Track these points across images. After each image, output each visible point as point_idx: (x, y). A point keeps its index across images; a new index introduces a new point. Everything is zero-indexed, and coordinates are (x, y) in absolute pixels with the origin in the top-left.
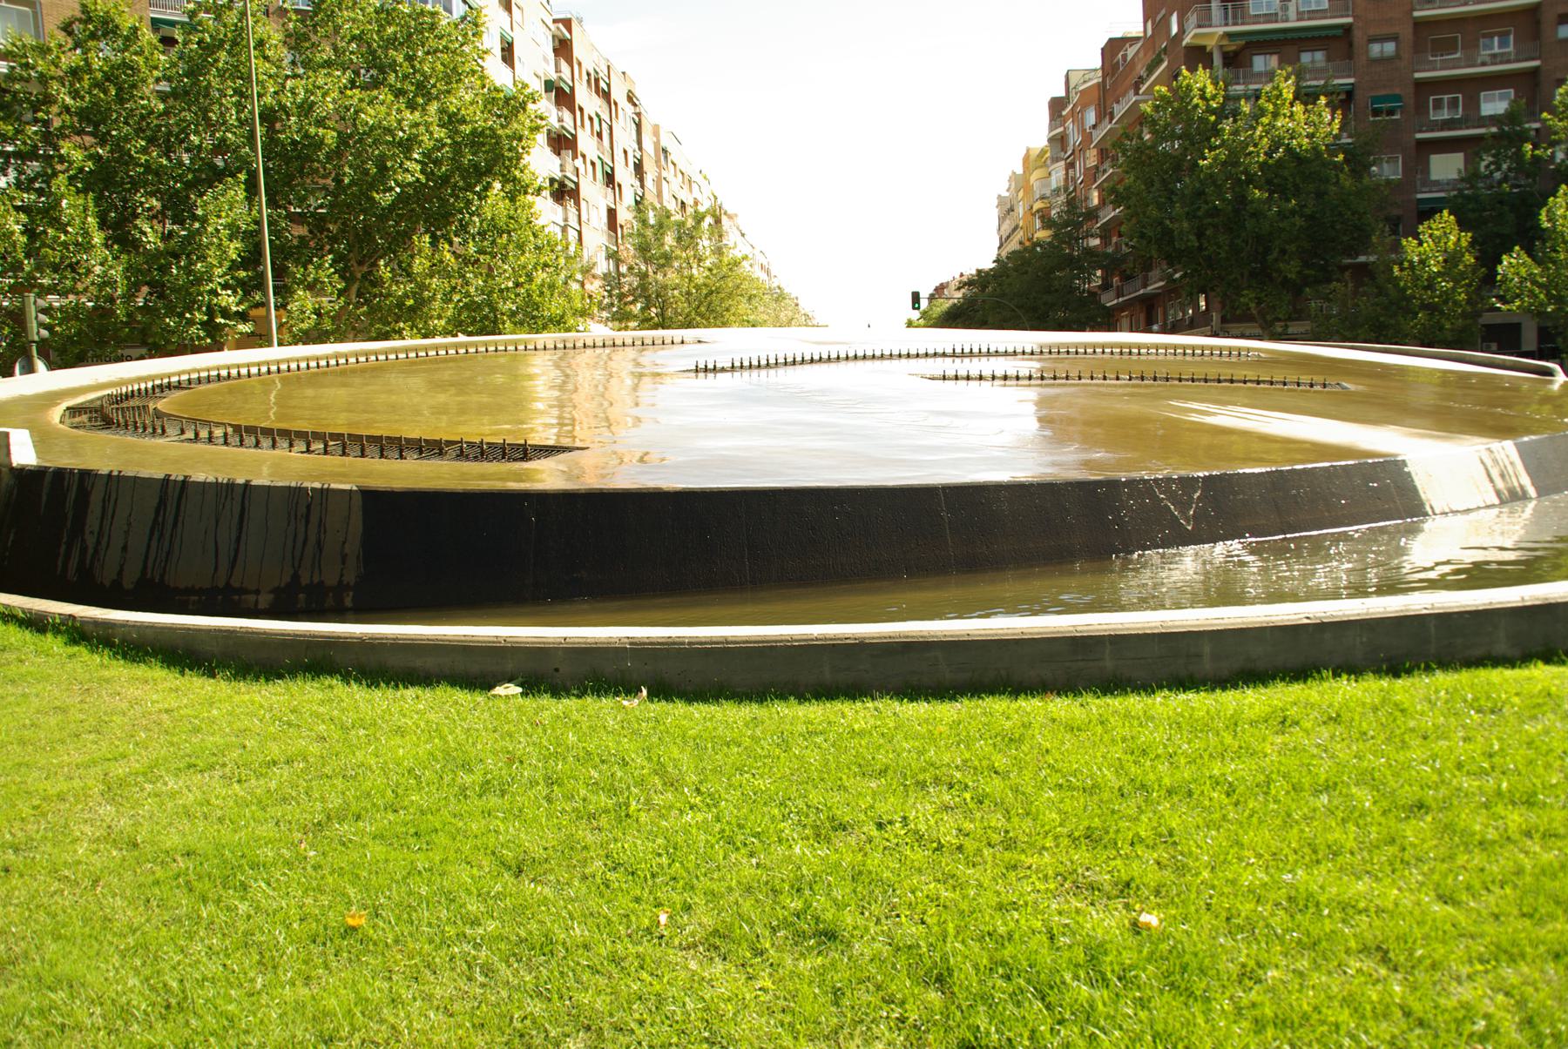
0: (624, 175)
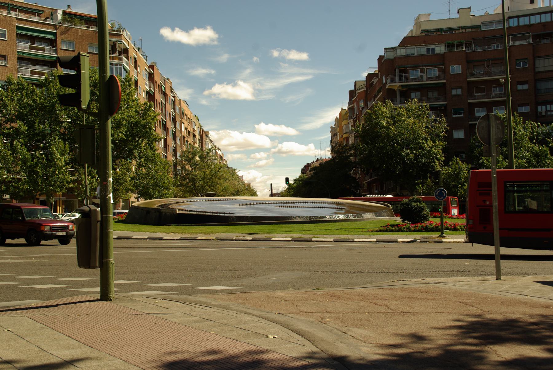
0: (170, 125)
